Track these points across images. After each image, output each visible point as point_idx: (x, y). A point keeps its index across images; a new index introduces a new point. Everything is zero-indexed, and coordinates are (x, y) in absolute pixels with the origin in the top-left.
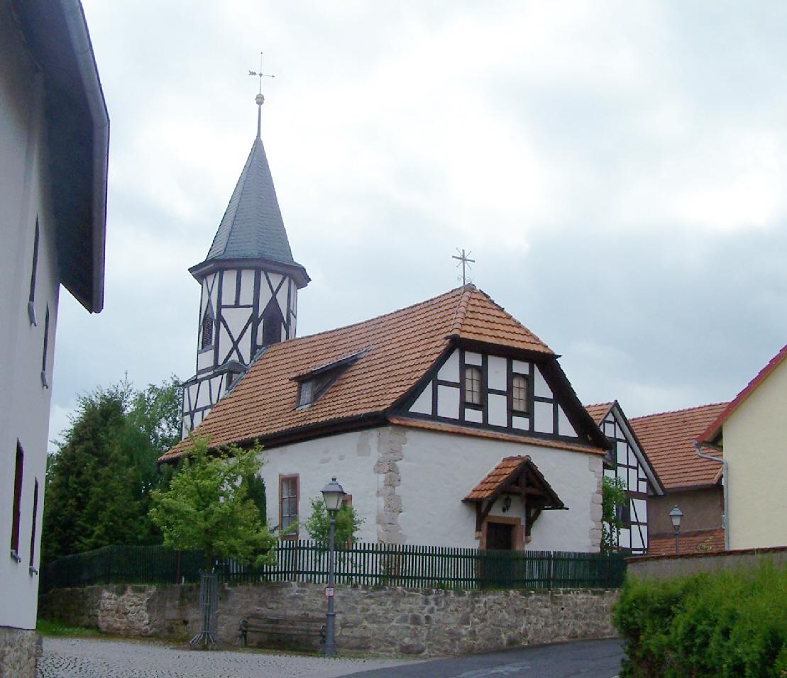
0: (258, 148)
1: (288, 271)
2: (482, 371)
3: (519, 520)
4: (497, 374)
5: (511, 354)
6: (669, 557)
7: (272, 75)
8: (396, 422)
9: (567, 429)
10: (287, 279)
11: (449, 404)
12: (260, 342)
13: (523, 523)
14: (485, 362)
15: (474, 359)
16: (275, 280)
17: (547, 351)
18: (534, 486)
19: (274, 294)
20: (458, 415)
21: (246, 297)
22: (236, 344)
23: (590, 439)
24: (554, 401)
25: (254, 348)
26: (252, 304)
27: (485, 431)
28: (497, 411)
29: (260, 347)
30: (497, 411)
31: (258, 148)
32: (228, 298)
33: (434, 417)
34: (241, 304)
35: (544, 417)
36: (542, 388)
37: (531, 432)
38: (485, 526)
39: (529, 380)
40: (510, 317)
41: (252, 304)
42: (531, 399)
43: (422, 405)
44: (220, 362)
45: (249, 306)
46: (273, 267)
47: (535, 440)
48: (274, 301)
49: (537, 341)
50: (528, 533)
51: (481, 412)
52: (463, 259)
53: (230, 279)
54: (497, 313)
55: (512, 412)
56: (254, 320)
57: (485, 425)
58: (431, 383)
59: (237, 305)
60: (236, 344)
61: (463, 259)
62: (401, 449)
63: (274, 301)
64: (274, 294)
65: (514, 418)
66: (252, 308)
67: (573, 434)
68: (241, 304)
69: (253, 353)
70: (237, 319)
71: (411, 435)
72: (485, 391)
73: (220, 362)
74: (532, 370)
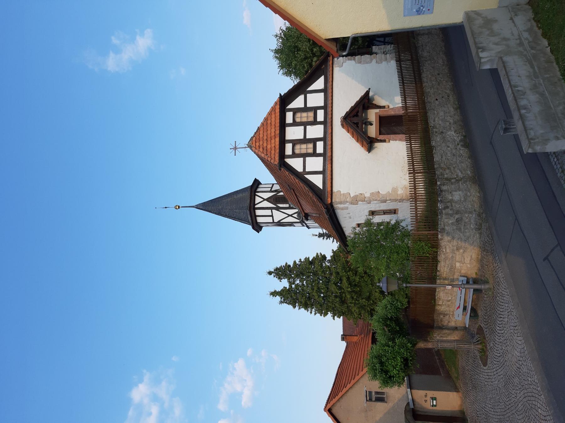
0: (198, 207)
1: (252, 207)
2: (295, 142)
3: (376, 113)
4: (294, 133)
5: (283, 125)
6: (494, 132)
7: (165, 207)
8: (329, 200)
9: (319, 84)
10: (257, 194)
11: (315, 164)
12: (287, 206)
13: (377, 111)
14: (290, 141)
15: (289, 150)
16: (258, 200)
17: (279, 103)
18: (358, 112)
19: (264, 200)
20: (319, 153)
21: (268, 212)
22: (289, 215)
23: (324, 66)
24: (305, 93)
25: (290, 208)
26: (271, 210)
27: (327, 139)
28: (316, 131)
29: (290, 205)
30: (316, 131)
31: (198, 207)
32: (270, 220)
33: (323, 173)
34: (271, 214)
35: (315, 100)
36: (298, 103)
37: (325, 108)
38: (382, 137)
39: (295, 111)
40: (263, 124)
41: (271, 210)
42: (306, 109)
43: (317, 180)
44: (299, 221)
45: (272, 212)
46: (253, 202)
47: (330, 105)
48: (268, 200)
49: (273, 109)
50: (384, 107)
51: (318, 143)
52: (235, 148)
53: (260, 220)
54: (261, 132)
55: (315, 122)
56: (278, 209)
57: (324, 139)
58: (305, 176)
59: (272, 216)
60: (289, 215)
61: (235, 148)
62: (344, 194)
63: (268, 200)
64: (264, 200)
65: (318, 120)
66: (273, 210)
67: (322, 79)
68: (271, 214)
69: (292, 208)
70: (278, 216)
71: (335, 190)
72: (305, 141)
73: (299, 221)
74: (290, 110)
